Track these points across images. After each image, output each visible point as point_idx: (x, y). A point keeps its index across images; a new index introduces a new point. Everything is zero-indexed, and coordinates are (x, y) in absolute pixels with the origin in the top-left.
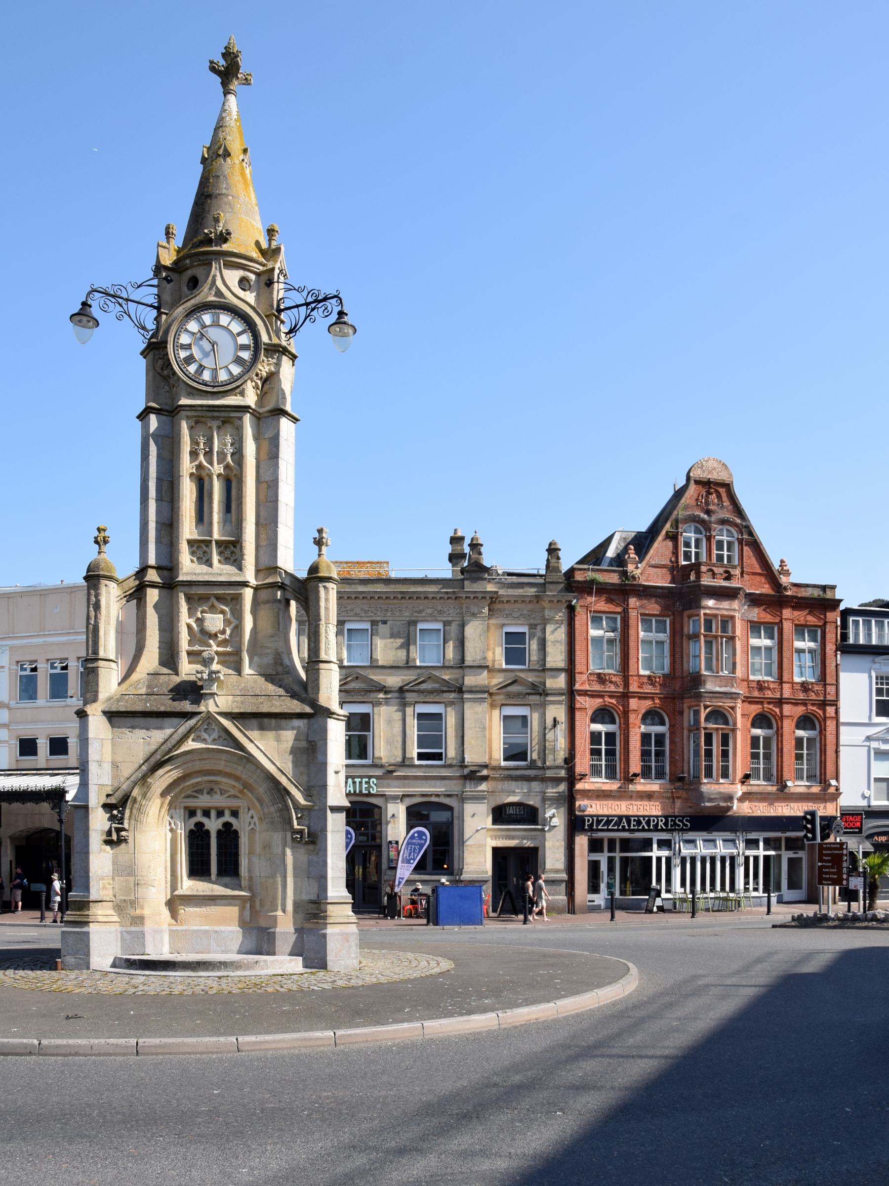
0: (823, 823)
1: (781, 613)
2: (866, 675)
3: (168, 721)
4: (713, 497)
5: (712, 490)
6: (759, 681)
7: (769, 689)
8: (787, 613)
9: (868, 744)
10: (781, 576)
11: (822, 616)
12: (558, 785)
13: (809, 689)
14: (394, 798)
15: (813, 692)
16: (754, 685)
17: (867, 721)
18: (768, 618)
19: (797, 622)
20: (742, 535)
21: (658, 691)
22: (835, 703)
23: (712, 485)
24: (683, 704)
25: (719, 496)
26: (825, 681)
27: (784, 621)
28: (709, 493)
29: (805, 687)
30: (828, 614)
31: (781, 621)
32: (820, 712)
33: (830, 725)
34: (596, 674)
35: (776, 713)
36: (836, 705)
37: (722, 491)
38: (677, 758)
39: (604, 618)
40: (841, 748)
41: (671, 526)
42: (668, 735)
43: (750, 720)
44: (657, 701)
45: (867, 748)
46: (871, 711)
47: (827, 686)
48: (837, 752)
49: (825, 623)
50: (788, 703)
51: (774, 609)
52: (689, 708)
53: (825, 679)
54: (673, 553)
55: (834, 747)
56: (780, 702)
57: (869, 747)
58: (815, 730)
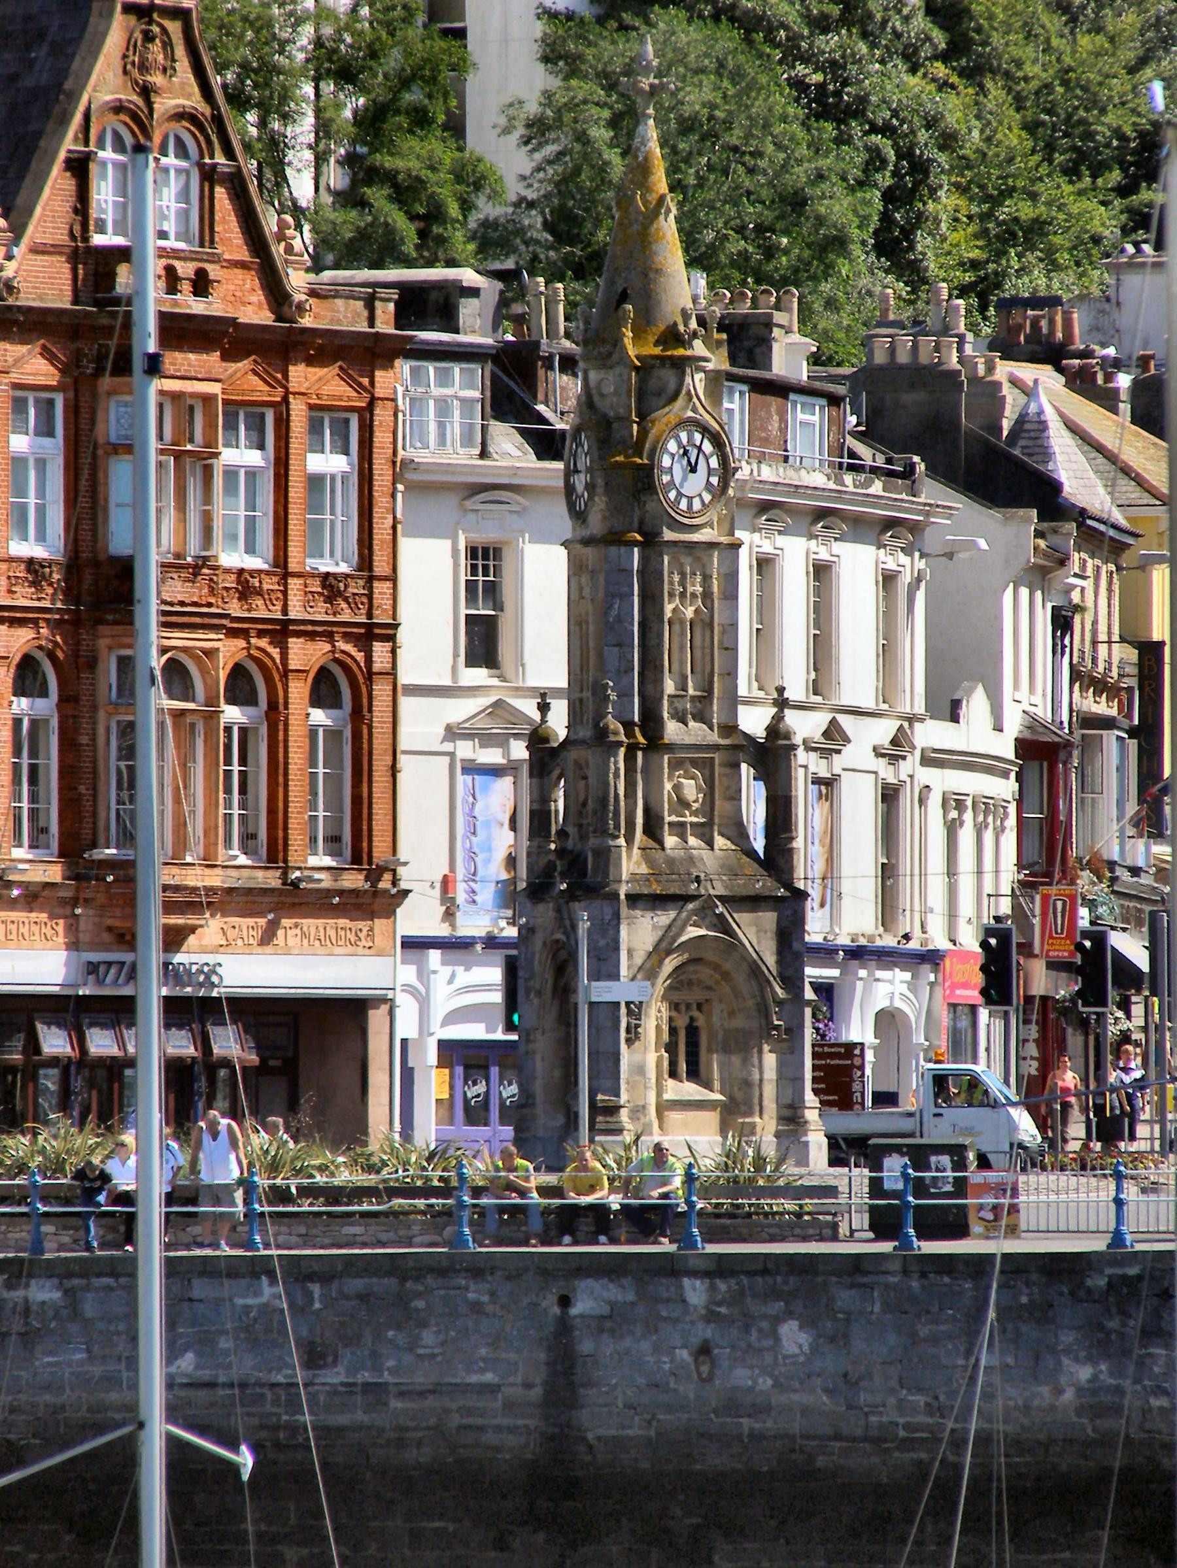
0: (817, 1074)
1: (286, 376)
2: (447, 543)
3: (670, 905)
4: (156, 48)
5: (156, 29)
6: (241, 571)
7: (259, 592)
8: (300, 375)
9: (448, 747)
10: (290, 271)
11: (365, 381)
12: (1071, 1106)
13: (340, 594)
14: (659, 1094)
15: (346, 600)
16: (230, 582)
17: (447, 681)
18: (256, 388)
19: (314, 401)
20: (212, 157)
21: (46, 604)
22: (389, 634)
23: (155, 16)
24: (95, 637)
25: (168, 45)
26: (370, 569)
27: (291, 398)
28: (148, 37)
29: (331, 587)
30: (379, 374)
31: (285, 400)
32: (275, 652)
33: (381, 689)
34: (319, 575)
35: (273, 659)
36: (394, 642)
37: (174, 27)
38: (82, 789)
39: (31, 402)
40: (402, 760)
41: (76, 139)
42: (55, 723)
43: (310, 680)
44: (44, 631)
45: (447, 759)
46: (456, 655)
47: (376, 584)
48: (394, 770)
49: (373, 401)
50: (298, 634)
51: (269, 365)
52: (110, 648)
53: (371, 561)
54: (76, 211)
55: (388, 760)
56: (281, 631)
57: (452, 755)
58: (43, 693)
